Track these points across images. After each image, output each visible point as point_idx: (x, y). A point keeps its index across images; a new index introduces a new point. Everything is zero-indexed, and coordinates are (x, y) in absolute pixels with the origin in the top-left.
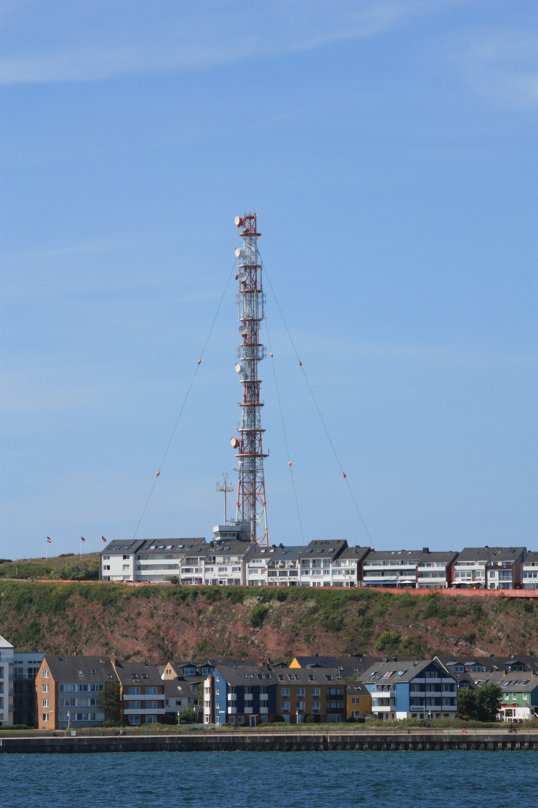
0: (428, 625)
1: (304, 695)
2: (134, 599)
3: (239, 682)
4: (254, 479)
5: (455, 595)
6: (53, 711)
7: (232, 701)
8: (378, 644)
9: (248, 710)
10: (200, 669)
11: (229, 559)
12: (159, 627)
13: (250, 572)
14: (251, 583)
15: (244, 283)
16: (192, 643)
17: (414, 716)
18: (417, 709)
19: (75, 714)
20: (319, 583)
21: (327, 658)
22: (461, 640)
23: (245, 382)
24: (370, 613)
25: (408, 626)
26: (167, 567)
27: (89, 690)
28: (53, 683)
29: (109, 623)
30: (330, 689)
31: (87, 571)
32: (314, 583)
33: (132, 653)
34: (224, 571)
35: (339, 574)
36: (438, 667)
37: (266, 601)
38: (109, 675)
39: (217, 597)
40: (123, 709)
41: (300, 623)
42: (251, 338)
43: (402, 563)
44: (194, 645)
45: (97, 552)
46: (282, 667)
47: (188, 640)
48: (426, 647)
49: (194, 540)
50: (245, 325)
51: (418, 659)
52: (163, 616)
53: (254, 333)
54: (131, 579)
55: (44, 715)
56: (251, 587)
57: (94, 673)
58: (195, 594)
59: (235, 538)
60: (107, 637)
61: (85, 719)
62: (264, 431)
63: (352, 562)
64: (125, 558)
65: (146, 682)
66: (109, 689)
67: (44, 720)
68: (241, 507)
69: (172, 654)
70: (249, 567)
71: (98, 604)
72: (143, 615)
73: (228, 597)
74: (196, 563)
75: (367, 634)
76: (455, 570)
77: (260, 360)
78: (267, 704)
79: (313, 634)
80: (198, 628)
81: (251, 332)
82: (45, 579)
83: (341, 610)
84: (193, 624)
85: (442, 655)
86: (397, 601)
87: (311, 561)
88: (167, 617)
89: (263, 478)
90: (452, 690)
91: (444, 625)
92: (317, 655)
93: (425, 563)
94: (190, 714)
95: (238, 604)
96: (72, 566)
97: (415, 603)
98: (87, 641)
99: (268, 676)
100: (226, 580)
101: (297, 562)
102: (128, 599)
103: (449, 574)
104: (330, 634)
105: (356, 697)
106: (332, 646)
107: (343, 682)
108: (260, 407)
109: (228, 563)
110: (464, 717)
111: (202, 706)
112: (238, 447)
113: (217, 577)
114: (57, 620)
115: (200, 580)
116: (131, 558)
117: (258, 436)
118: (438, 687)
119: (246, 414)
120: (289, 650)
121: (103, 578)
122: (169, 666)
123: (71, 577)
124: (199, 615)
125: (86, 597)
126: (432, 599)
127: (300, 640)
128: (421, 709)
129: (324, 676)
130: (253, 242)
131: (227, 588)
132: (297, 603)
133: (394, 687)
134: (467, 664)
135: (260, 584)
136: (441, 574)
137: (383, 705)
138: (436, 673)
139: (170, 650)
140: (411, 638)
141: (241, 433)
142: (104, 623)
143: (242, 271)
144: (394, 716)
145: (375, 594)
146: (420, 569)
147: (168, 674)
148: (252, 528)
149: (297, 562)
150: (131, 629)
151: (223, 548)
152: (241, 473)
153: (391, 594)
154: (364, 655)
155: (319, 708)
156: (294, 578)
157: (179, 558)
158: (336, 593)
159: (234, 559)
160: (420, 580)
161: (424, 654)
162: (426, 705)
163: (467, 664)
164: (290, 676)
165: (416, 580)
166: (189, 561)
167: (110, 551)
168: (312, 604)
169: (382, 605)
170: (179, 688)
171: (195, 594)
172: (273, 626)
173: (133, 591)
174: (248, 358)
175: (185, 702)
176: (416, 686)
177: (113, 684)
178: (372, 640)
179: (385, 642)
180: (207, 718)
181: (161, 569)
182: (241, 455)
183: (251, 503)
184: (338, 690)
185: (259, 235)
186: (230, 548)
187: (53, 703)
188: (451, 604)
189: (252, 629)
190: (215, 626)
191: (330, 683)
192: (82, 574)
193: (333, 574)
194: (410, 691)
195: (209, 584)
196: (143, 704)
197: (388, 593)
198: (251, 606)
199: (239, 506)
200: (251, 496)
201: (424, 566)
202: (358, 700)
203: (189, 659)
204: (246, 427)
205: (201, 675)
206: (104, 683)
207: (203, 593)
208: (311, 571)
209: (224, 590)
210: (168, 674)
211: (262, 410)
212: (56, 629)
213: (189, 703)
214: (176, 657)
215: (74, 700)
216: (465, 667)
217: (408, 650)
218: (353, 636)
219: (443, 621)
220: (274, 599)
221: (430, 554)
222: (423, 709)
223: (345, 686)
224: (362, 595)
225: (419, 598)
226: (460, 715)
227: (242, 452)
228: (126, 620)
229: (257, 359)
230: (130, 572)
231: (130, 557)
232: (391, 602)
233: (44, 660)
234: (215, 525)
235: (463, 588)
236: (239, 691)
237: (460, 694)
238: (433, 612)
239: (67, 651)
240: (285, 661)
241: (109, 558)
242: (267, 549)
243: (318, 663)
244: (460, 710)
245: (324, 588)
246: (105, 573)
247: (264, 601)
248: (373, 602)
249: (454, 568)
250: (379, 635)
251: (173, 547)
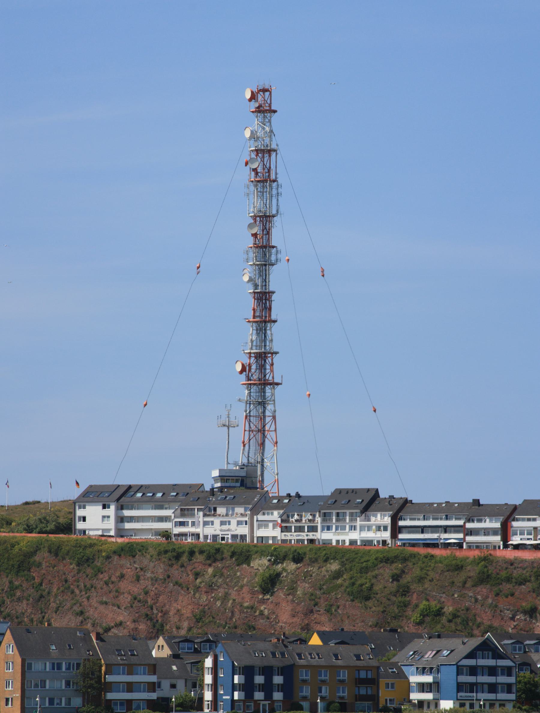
0: (478, 593)
1: (328, 678)
2: (116, 558)
3: (248, 662)
4: (264, 412)
5: (512, 557)
6: (18, 695)
7: (240, 684)
8: (415, 616)
9: (259, 695)
10: (199, 644)
11: (233, 510)
12: (146, 593)
13: (259, 527)
14: (260, 539)
15: (255, 170)
16: (187, 612)
17: (462, 705)
18: (466, 696)
19: (45, 699)
20: (344, 541)
21: (355, 633)
22: (518, 613)
23: (254, 293)
24: (406, 579)
25: (453, 595)
26: (156, 519)
27: (64, 669)
28: (19, 660)
29: (85, 586)
30: (359, 671)
31: (57, 523)
32: (338, 541)
33: (112, 624)
34: (228, 525)
35: (368, 530)
36: (493, 646)
37: (279, 563)
38: (89, 651)
39: (218, 556)
40: (106, 692)
41: (320, 590)
42: (262, 237)
43: (447, 518)
44: (189, 615)
45: (68, 499)
46: (300, 643)
47: (181, 608)
48: (475, 621)
49: (191, 486)
50: (255, 222)
51: (466, 637)
52: (152, 579)
53: (267, 232)
54: (112, 533)
55: (7, 700)
56: (260, 544)
57: (70, 648)
58: (192, 553)
59: (238, 484)
60: (83, 604)
61: (57, 704)
62: (276, 353)
63: (385, 516)
64: (104, 507)
65: (134, 660)
66: (88, 668)
67: (7, 705)
68: (247, 446)
69: (162, 626)
70: (257, 521)
71: (71, 564)
72: (126, 577)
73: (232, 557)
74: (193, 515)
75: (402, 605)
76: (512, 527)
77: (273, 265)
78: (281, 688)
79: (336, 604)
80: (194, 594)
81: (263, 231)
82: (4, 532)
83: (370, 574)
84: (188, 589)
85: (495, 631)
86: (440, 565)
87: (334, 514)
88: (156, 580)
89: (275, 411)
90: (509, 675)
91: (497, 595)
92: (342, 630)
93: (476, 518)
94: (187, 699)
95: (244, 566)
96: (39, 516)
97: (462, 567)
98: (57, 609)
99: (283, 654)
100: (229, 536)
101: (317, 515)
102: (108, 557)
103: (505, 532)
104: (357, 603)
105: (390, 681)
106: (359, 618)
107: (374, 663)
108: (273, 324)
109: (232, 515)
110: (523, 708)
111: (201, 691)
112: (244, 373)
113: (218, 532)
114: (19, 582)
115: (198, 535)
116: (113, 507)
117: (270, 359)
118: (492, 671)
119: (255, 332)
120: (307, 622)
121: (77, 532)
122: (161, 641)
123: (38, 530)
124: (196, 579)
125: (56, 555)
126: (483, 563)
127: (320, 611)
128: (470, 697)
129: (352, 654)
130: (267, 120)
131: (231, 545)
132: (317, 565)
133: (438, 669)
134: (528, 642)
135: (271, 542)
136: (494, 532)
137: (423, 692)
138: (490, 653)
139: (160, 621)
140: (456, 610)
141: (248, 355)
142: (78, 586)
143: (253, 155)
144: (437, 705)
145: (413, 555)
146: (469, 525)
147: (160, 650)
148: (259, 473)
149: (317, 515)
150: (111, 595)
151: (226, 497)
152: (248, 405)
153: (432, 556)
154: (399, 630)
155: (346, 694)
156: (313, 535)
157: (172, 509)
158: (364, 554)
159: (240, 510)
160: (469, 539)
161: (472, 630)
162: (477, 692)
163: (528, 642)
164: (310, 654)
165: (464, 539)
166: (184, 512)
167: (86, 499)
168: (334, 566)
169: (422, 569)
170: (174, 668)
171: (192, 553)
172: (287, 593)
173: (114, 548)
174: (258, 263)
175: (181, 684)
176: (465, 668)
177: (93, 662)
178: (409, 612)
179: (424, 615)
180: (208, 704)
181: (149, 522)
182: (247, 382)
183: (260, 442)
184: (369, 673)
185: (275, 111)
186: (234, 497)
187: (18, 685)
188: (507, 568)
189: (260, 597)
190: (215, 592)
191: (359, 663)
192: (51, 526)
193: (361, 531)
194: (458, 674)
195: (208, 541)
196: (130, 687)
197: (429, 554)
198: (260, 568)
199: (244, 446)
200: (259, 433)
201: (473, 521)
202: (393, 684)
203: (183, 632)
204: (254, 348)
205: (200, 652)
206: (82, 661)
207: (201, 552)
208: (334, 527)
209: (227, 548)
210: (160, 650)
211: (275, 326)
212: (18, 594)
213: (186, 686)
214: (167, 630)
215: (45, 681)
216: (524, 646)
217: (453, 625)
218: (385, 607)
219: (496, 589)
220: (289, 560)
221: (480, 507)
222: (473, 696)
223: (378, 668)
224: (396, 557)
225: (467, 561)
226: (518, 705)
227: (249, 379)
228: (107, 583)
229: (269, 265)
230: (111, 525)
231: (111, 507)
232: (433, 565)
233: (8, 631)
234: (214, 469)
235: (522, 549)
236: (248, 672)
237: (518, 679)
238: (484, 578)
239: (32, 621)
240: (303, 635)
241: (84, 508)
242: (280, 499)
243: (344, 638)
244: (518, 698)
245: (350, 547)
246: (80, 526)
247: (275, 563)
248: (410, 564)
249: (511, 524)
250: (417, 606)
251: (164, 494)
